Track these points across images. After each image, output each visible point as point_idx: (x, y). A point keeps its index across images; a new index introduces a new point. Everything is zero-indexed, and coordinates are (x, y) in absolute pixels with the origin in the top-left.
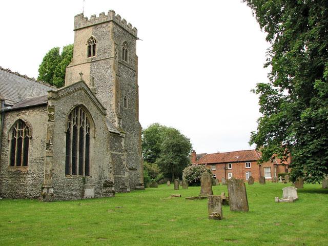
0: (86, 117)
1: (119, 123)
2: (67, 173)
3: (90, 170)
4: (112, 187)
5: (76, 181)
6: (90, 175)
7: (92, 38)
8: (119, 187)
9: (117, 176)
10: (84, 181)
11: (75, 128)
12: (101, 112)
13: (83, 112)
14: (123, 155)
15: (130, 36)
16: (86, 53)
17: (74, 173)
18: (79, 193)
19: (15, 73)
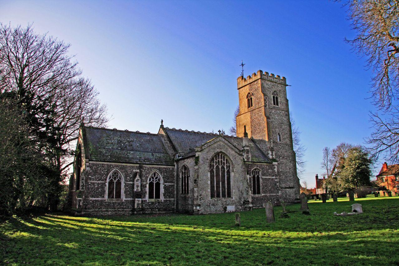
0: (226, 159)
1: (272, 155)
2: (212, 196)
3: (232, 194)
4: (249, 204)
6: (232, 197)
8: (274, 203)
9: (271, 194)
12: (239, 154)
13: (223, 156)
14: (277, 179)
17: (218, 196)
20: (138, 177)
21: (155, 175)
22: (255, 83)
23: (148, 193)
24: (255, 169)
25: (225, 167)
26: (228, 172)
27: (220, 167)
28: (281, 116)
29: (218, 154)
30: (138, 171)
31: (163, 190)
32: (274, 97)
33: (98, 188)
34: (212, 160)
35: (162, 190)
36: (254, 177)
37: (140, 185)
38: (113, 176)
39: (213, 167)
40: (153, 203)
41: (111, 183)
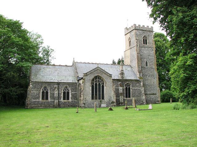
2: (92, 99)
10: (101, 101)
11: (96, 84)
12: (109, 76)
15: (148, 32)
19: (84, 63)
20: (56, 89)
21: (66, 88)
22: (132, 31)
23: (62, 97)
24: (128, 84)
25: (101, 84)
26: (103, 87)
27: (98, 84)
28: (149, 51)
29: (97, 77)
30: (57, 86)
31: (71, 95)
32: (144, 40)
33: (36, 95)
34: (93, 80)
35: (70, 96)
36: (126, 88)
37: (57, 93)
38: (44, 89)
39: (94, 84)
40: (65, 102)
41: (43, 92)
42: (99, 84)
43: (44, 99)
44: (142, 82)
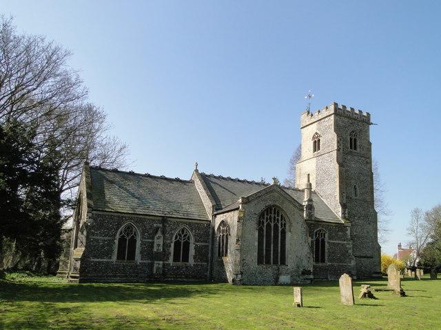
2: (260, 262)
5: (270, 271)
7: (317, 133)
9: (150, 241)
11: (269, 225)
16: (312, 149)
17: (268, 262)
18: (272, 280)
20: (159, 234)
23: (172, 254)
26: (284, 233)
27: (272, 225)
30: (161, 225)
31: (194, 251)
32: (351, 139)
33: (103, 246)
34: (262, 215)
35: (192, 252)
38: (125, 231)
40: (178, 268)
41: (122, 240)
42: (276, 227)
43: (124, 259)
44: (349, 229)
